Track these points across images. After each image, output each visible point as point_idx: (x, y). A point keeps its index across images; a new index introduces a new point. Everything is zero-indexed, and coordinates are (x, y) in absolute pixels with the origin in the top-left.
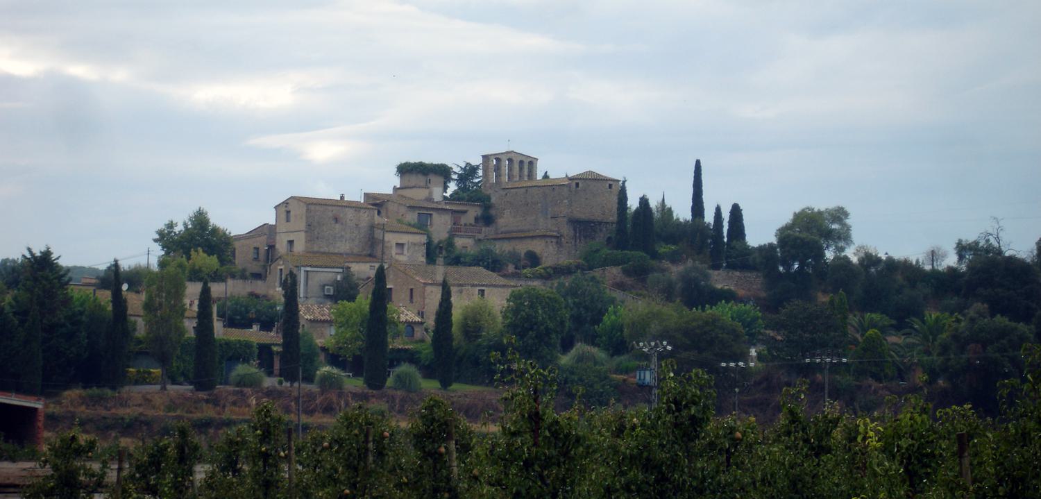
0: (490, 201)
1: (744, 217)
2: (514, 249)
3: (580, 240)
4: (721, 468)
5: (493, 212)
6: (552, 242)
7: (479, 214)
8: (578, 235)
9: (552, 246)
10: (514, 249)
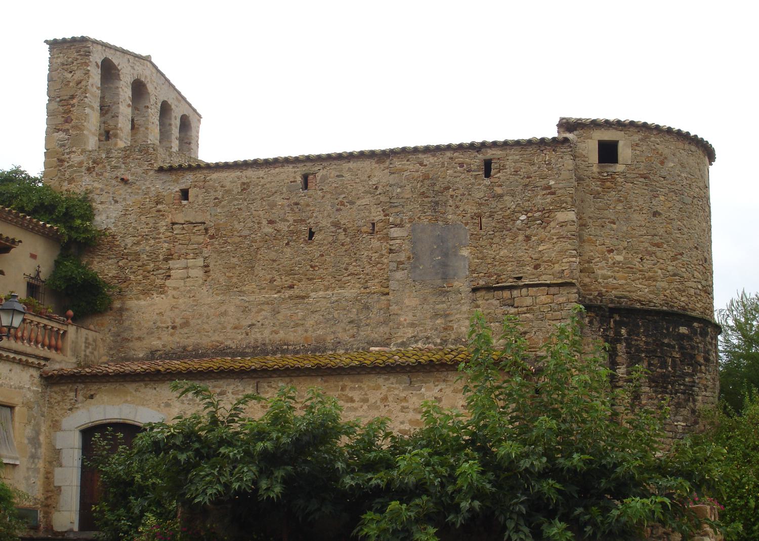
4: (235, 341)
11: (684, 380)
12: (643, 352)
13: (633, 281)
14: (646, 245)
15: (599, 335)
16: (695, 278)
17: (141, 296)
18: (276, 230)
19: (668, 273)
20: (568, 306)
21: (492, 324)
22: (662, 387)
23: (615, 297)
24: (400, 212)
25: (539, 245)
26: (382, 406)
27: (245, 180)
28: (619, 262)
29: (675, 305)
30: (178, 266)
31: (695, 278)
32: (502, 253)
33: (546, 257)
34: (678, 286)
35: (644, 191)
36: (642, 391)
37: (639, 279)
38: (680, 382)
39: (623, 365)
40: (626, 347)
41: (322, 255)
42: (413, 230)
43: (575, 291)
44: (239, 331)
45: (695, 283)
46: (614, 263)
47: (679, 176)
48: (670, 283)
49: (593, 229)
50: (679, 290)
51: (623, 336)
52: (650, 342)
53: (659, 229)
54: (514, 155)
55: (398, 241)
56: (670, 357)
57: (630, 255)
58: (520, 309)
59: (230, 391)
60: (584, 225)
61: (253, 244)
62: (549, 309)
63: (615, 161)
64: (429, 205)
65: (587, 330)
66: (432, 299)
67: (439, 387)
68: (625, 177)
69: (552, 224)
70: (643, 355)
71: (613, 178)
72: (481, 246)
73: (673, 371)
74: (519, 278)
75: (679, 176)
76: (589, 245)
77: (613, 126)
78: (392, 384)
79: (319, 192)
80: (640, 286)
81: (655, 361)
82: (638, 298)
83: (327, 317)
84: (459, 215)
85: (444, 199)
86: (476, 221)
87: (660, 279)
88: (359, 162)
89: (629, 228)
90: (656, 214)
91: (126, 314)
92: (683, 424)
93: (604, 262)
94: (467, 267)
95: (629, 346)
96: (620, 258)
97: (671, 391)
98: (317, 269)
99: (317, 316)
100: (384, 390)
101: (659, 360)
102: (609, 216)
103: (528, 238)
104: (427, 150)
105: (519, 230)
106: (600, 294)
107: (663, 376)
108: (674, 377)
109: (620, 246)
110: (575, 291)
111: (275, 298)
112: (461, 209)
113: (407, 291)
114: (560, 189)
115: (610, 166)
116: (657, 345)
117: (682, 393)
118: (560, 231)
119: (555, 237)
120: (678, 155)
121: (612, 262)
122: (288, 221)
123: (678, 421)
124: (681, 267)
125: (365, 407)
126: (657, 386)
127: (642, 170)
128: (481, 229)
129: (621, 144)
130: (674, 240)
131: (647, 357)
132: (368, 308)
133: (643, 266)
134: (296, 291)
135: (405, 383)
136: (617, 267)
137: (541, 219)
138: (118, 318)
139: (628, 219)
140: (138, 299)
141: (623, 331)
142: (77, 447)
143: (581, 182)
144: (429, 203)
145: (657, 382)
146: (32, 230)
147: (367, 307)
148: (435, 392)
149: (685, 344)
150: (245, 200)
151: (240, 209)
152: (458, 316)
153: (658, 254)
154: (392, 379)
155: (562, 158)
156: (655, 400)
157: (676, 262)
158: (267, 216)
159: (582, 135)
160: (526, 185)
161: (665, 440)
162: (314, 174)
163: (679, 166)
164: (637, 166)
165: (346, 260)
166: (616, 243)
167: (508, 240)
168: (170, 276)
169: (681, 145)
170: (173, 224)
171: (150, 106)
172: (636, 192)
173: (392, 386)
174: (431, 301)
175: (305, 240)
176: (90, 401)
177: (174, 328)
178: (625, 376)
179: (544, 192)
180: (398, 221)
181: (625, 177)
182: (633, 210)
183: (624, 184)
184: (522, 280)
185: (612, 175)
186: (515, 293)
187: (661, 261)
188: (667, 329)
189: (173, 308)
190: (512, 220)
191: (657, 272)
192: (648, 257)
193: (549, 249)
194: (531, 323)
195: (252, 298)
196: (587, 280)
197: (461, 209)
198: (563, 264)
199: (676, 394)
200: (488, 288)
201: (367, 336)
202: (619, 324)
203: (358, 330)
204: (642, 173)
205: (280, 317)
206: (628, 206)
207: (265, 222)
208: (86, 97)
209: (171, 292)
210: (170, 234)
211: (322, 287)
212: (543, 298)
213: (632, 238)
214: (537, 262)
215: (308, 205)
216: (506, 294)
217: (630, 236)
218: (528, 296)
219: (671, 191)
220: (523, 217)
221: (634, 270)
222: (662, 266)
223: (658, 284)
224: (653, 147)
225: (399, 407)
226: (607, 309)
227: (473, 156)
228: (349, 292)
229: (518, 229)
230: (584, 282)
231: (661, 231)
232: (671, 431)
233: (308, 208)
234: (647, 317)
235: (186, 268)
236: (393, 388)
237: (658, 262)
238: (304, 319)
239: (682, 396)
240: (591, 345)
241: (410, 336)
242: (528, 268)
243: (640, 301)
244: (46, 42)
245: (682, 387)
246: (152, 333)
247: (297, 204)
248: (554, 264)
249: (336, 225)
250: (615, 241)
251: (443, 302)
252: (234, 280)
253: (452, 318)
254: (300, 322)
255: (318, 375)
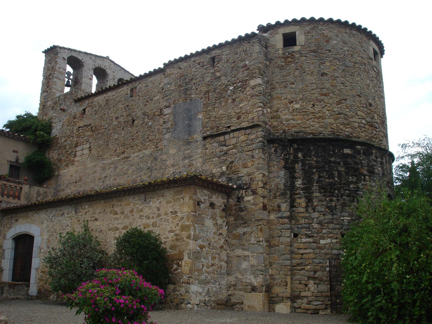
0: (49, 133)
1: (394, 155)
2: (86, 229)
3: (309, 200)
4: (98, 186)
5: (53, 155)
6: (212, 205)
7: (22, 160)
8: (299, 183)
9: (213, 218)
10: (86, 229)
11: (349, 187)
12: (314, 168)
13: (307, 120)
14: (316, 95)
15: (281, 159)
16: (358, 116)
17: (65, 167)
18: (118, 122)
19: (334, 113)
20: (257, 140)
21: (214, 159)
22: (330, 192)
23: (295, 132)
24: (169, 99)
25: (240, 103)
26: (131, 216)
27: (107, 98)
28: (297, 109)
29: (341, 134)
30: (79, 149)
31: (358, 116)
32: (219, 113)
33: (244, 111)
34: (343, 121)
35: (314, 61)
36: (314, 196)
37: (311, 119)
38: (345, 188)
39: (300, 178)
40: (302, 166)
41: (137, 132)
42: (175, 108)
43: (261, 129)
44: (100, 181)
45: (359, 119)
46: (293, 110)
47: (341, 49)
48: (336, 119)
49: (279, 90)
50: (344, 124)
51: (300, 158)
52: (320, 161)
53: (327, 84)
54: (226, 51)
55: (167, 116)
56: (336, 171)
57: (305, 104)
58: (229, 147)
59: (66, 213)
60: (274, 88)
61: (109, 132)
62: (246, 145)
63: (295, 44)
64: (183, 91)
65: (273, 157)
66: (183, 148)
67: (159, 201)
68: (301, 53)
69: (248, 89)
70: (314, 170)
71: (292, 55)
72: (209, 111)
73: (339, 180)
74: (229, 127)
75: (341, 49)
76: (277, 100)
77: (292, 24)
78: (136, 201)
79: (137, 97)
80: (313, 123)
81: (325, 174)
82: (311, 131)
83: (138, 167)
84: (198, 94)
85: (190, 86)
86: (206, 96)
87: (327, 117)
88: (155, 77)
89: (303, 86)
90: (323, 74)
91: (59, 177)
92: (348, 218)
93: (287, 110)
94: (201, 125)
95: (304, 164)
96: (297, 106)
97: (338, 195)
98: (135, 140)
99: (133, 167)
100: (132, 205)
101: (327, 173)
102: (290, 80)
103: (234, 100)
104: (181, 59)
105: (229, 96)
106: (284, 132)
107: (330, 184)
108: (340, 185)
109: (298, 98)
110: (261, 129)
111: (116, 160)
112: (199, 90)
113: (171, 145)
114: (252, 65)
115: (290, 48)
116: (325, 162)
117: (347, 196)
118: (252, 92)
119: (249, 97)
120: (340, 35)
121: (292, 109)
122: (124, 116)
123: (343, 217)
124: (345, 109)
125: (122, 217)
126: (325, 192)
127: (313, 48)
128: (209, 100)
129: (297, 33)
130: (338, 91)
131: (318, 171)
132: (156, 159)
133: (315, 110)
134: (126, 155)
135: (142, 200)
136: (295, 112)
137: (241, 87)
138: (56, 180)
139: (303, 81)
140: (64, 169)
141: (300, 155)
142: (10, 248)
143: (272, 61)
144: (183, 90)
145: (325, 189)
146: (14, 139)
147: (155, 159)
148: (157, 204)
149: (349, 161)
150: (107, 109)
151: (104, 114)
152: (196, 156)
153: (326, 100)
154: (137, 198)
155: (253, 46)
156: (324, 202)
157: (340, 105)
158: (115, 115)
159: (272, 33)
160: (233, 68)
161: (333, 231)
162: (136, 88)
163: (341, 43)
164: (309, 45)
165: (148, 133)
166: (294, 96)
167: (223, 104)
168: (76, 155)
169: (343, 30)
170: (80, 127)
171: (109, 80)
172: (308, 62)
173: (136, 202)
174: (183, 149)
175: (130, 125)
176: (16, 222)
177: (76, 182)
178: (301, 186)
179: (243, 69)
180: (168, 104)
181: (301, 53)
182: (306, 74)
183: (300, 58)
184: (231, 128)
185: (292, 55)
186: (227, 137)
187: (328, 105)
188: (334, 151)
189: (77, 171)
190: (226, 91)
191: (325, 113)
192: (318, 104)
193: (246, 105)
194: (235, 155)
195: (106, 162)
196: (275, 124)
197: (199, 90)
198: (254, 113)
199: (342, 197)
200: (212, 136)
201: (155, 176)
202: (296, 151)
203: (151, 173)
204: (312, 49)
205: (117, 170)
206: (303, 71)
207: (114, 119)
208: (54, 74)
209: (76, 164)
210: (77, 133)
211: (137, 150)
212: (242, 137)
213: (306, 92)
214: (239, 115)
215: (132, 106)
216: (222, 138)
217: (304, 91)
218: (234, 137)
219: (335, 59)
220: (231, 88)
221: (308, 113)
222: (329, 108)
223: (326, 121)
224: (321, 33)
225: (139, 216)
226: (286, 141)
227: (205, 57)
228: (147, 152)
229: (228, 96)
230: (274, 125)
231: (328, 85)
232: (338, 224)
233: (133, 107)
234: (317, 144)
235: (83, 150)
236: (136, 203)
237: (326, 106)
238: (128, 170)
239: (347, 198)
240: (276, 167)
241: (172, 173)
242: (234, 119)
243: (312, 134)
244: (43, 52)
245: (347, 192)
246: (68, 186)
247: (128, 106)
248: (248, 114)
249: (144, 114)
250: (294, 96)
251: (189, 149)
252: (100, 153)
253: (193, 159)
254: (126, 172)
255: (101, 199)
